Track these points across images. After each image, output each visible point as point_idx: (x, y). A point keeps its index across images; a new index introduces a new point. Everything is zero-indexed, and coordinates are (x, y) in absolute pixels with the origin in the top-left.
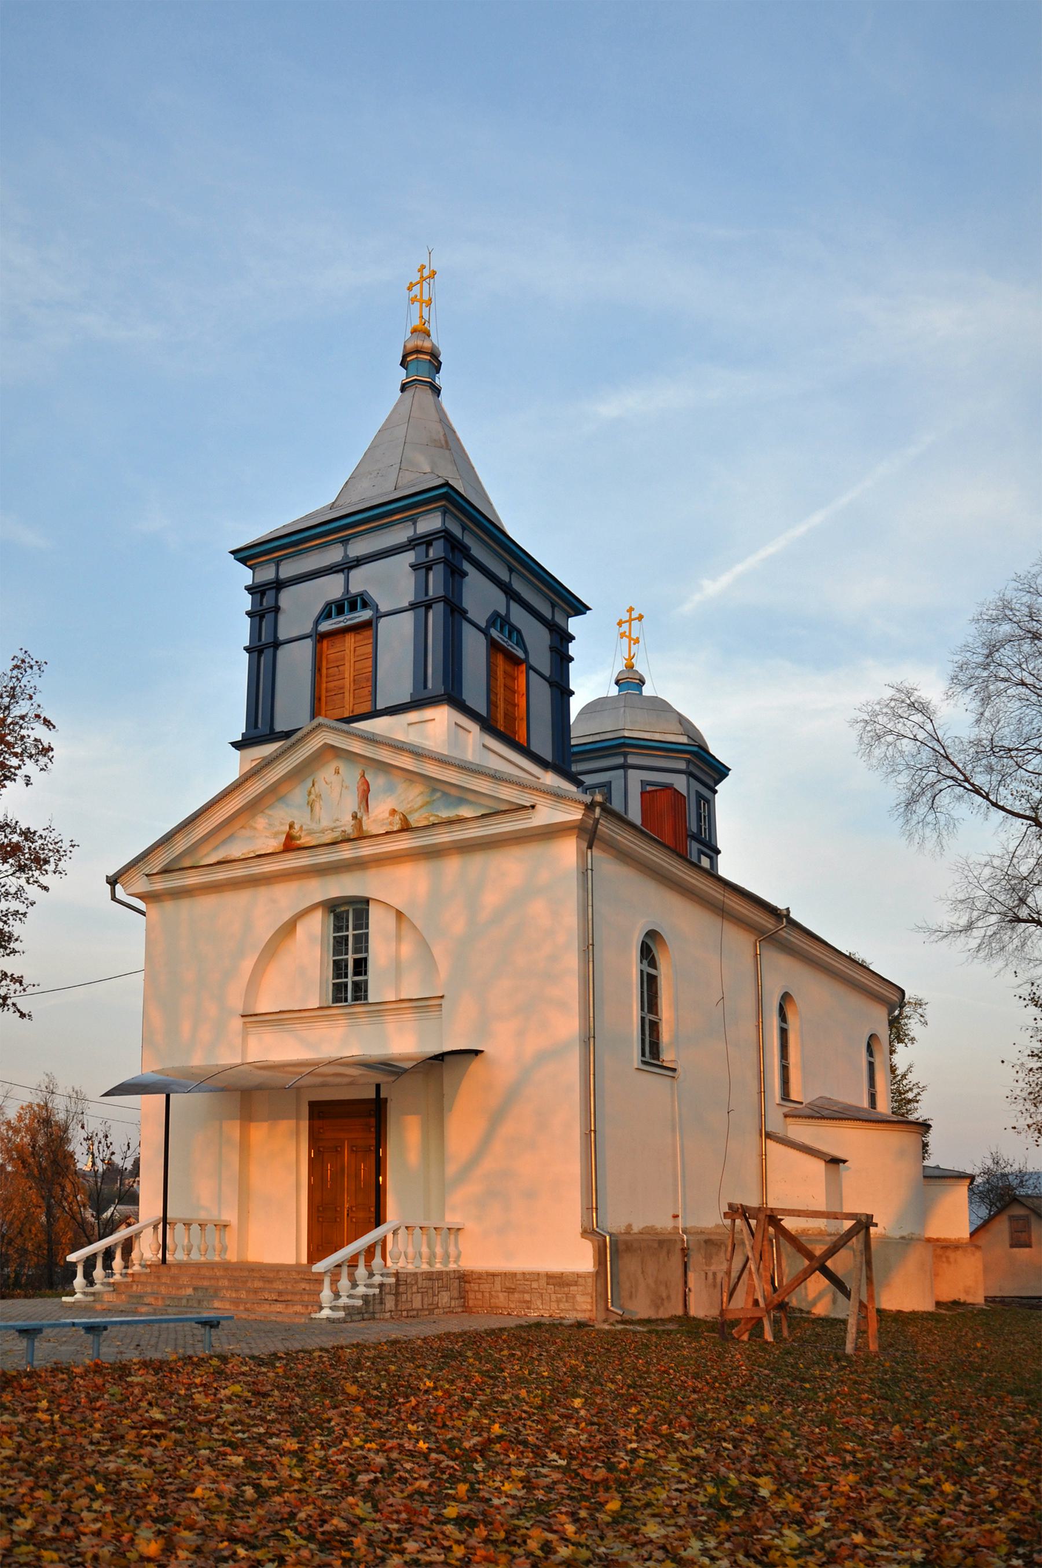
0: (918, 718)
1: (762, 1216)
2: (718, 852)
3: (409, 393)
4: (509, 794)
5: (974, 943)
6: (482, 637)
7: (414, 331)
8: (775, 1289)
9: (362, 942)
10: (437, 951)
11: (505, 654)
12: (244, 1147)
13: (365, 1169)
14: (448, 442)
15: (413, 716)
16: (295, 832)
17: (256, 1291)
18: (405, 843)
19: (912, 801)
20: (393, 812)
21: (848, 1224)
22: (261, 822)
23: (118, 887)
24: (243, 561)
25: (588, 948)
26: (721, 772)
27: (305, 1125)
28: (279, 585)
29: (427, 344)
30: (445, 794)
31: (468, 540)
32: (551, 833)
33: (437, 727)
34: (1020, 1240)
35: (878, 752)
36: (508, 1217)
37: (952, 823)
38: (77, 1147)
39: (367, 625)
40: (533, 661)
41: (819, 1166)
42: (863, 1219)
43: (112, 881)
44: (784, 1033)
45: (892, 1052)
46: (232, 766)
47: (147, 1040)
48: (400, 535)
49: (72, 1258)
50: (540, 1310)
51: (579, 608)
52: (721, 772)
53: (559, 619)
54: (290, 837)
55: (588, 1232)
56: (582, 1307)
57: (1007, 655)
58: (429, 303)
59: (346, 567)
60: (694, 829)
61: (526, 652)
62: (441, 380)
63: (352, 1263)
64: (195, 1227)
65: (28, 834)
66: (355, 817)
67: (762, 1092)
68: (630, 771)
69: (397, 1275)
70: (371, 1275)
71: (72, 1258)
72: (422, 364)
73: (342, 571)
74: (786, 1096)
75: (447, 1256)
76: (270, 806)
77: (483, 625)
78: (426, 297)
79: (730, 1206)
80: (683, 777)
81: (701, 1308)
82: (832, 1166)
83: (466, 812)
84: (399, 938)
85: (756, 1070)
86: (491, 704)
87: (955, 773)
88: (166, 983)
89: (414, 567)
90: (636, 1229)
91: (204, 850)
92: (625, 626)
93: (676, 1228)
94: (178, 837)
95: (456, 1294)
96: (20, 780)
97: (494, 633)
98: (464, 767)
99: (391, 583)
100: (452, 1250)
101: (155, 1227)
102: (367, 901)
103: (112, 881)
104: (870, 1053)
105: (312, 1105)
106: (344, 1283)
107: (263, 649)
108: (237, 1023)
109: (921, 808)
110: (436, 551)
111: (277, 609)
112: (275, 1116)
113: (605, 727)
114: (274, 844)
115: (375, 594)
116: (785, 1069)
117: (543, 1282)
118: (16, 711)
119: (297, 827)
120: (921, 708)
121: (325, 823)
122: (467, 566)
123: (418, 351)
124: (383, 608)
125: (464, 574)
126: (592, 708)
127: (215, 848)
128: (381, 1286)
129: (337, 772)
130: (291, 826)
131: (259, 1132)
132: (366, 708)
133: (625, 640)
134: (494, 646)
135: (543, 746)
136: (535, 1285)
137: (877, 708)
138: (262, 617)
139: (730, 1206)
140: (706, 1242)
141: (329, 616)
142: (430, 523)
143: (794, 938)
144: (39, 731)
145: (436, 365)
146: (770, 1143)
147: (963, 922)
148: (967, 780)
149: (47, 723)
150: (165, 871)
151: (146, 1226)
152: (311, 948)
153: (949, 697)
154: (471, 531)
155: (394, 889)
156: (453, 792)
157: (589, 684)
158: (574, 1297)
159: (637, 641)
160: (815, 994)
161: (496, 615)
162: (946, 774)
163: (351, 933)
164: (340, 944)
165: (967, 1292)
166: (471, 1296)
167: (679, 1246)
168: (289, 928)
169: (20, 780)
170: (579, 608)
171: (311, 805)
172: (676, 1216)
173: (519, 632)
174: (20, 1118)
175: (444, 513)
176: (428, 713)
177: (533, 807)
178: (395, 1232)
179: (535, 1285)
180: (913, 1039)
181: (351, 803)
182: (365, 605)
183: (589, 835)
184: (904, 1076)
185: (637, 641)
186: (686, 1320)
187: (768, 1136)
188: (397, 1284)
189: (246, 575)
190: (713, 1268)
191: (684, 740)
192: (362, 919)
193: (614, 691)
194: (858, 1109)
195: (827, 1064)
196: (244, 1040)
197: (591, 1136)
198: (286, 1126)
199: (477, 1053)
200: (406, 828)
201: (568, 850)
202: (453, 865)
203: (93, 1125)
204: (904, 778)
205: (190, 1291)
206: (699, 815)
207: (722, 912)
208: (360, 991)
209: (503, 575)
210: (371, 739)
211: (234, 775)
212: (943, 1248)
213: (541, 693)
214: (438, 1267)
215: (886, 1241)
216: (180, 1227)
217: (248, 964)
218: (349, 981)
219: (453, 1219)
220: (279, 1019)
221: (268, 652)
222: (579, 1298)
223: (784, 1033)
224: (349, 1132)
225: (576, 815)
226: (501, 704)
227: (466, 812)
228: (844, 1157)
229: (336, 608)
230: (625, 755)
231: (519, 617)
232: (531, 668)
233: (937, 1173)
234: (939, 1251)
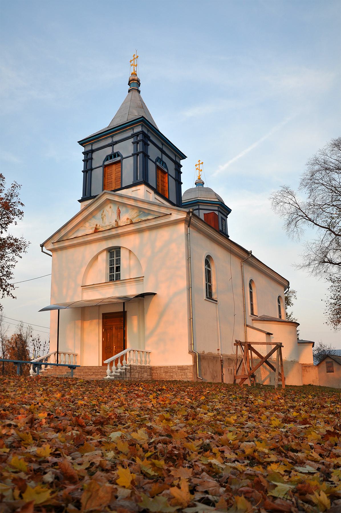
0: (290, 197)
1: (246, 345)
3: (131, 93)
4: (163, 211)
5: (311, 270)
7: (132, 74)
8: (251, 369)
9: (118, 261)
10: (142, 262)
11: (161, 170)
12: (82, 329)
13: (120, 335)
14: (143, 106)
15: (134, 188)
16: (98, 227)
17: (86, 372)
18: (132, 228)
19: (289, 224)
20: (128, 219)
21: (274, 346)
22: (87, 225)
23: (44, 247)
24: (81, 144)
25: (189, 259)
26: (229, 211)
27: (101, 321)
28: (92, 151)
29: (136, 78)
30: (144, 212)
31: (149, 135)
32: (176, 222)
33: (141, 192)
34: (330, 370)
35: (278, 208)
36: (164, 346)
37: (302, 231)
38: (30, 348)
39: (119, 162)
40: (169, 173)
42: (279, 344)
43: (42, 246)
44: (251, 293)
45: (286, 308)
46: (79, 207)
47: (52, 295)
48: (129, 134)
50: (176, 378)
51: (184, 157)
52: (229, 211)
53: (177, 160)
54: (96, 229)
55: (190, 352)
56: (189, 377)
57: (318, 175)
58: (136, 66)
60: (221, 229)
61: (167, 170)
62: (140, 88)
63: (116, 361)
64: (67, 355)
65: (16, 240)
66: (116, 221)
67: (245, 311)
69: (130, 366)
70: (122, 366)
72: (134, 84)
74: (252, 314)
75: (146, 361)
76: (90, 219)
77: (154, 161)
78: (135, 64)
79: (236, 341)
81: (228, 380)
83: (150, 217)
84: (130, 259)
85: (243, 304)
86: (157, 185)
87: (302, 214)
88: (58, 278)
89: (133, 143)
90: (206, 353)
91: (70, 234)
93: (219, 354)
94: (62, 230)
96: (14, 223)
97: (158, 163)
98: (150, 203)
99: (127, 148)
100: (147, 359)
101: (55, 354)
102: (119, 248)
103: (42, 246)
104: (279, 302)
105: (103, 314)
106: (114, 367)
107: (88, 171)
108: (80, 289)
109: (292, 226)
110: (140, 137)
111: (92, 159)
112: (92, 318)
113: (192, 197)
114: (92, 231)
115: (121, 152)
116: (252, 305)
117: (177, 369)
118: (12, 201)
119: (98, 225)
120: (291, 193)
121: (107, 223)
122: (149, 143)
123: (133, 80)
124: (124, 156)
125: (149, 145)
126: (188, 192)
127: (73, 234)
128: (126, 369)
129: (110, 208)
130: (96, 225)
131: (87, 324)
132: (119, 187)
133: (198, 171)
134: (158, 167)
135: (173, 199)
136: (174, 370)
137: (277, 194)
138: (87, 161)
139: (236, 341)
140: (228, 359)
141: (107, 160)
142: (138, 129)
143: (254, 261)
144: (19, 207)
145: (139, 84)
147: (307, 263)
148: (306, 216)
149: (22, 204)
150: (58, 241)
151: (52, 354)
152: (103, 264)
153: (300, 189)
154: (151, 132)
155: (127, 243)
156: (146, 211)
157: (187, 184)
158: (187, 373)
159: (201, 171)
160: (261, 281)
161: (158, 158)
162: (299, 215)
163: (115, 258)
164: (111, 262)
165: (313, 382)
166: (154, 375)
167: (220, 359)
168: (96, 258)
169: (14, 223)
170: (184, 157)
171: (103, 218)
172: (218, 350)
173: (165, 164)
174: (12, 339)
175: (142, 126)
176: (138, 187)
177: (171, 214)
178: (130, 352)
179: (174, 370)
180: (292, 304)
181: (115, 217)
182: (118, 156)
183: (188, 223)
184: (290, 316)
185: (201, 171)
186: (222, 384)
187: (247, 326)
188: (131, 369)
189: (83, 149)
190: (231, 368)
191: (217, 200)
192: (118, 254)
193: (195, 186)
194: (276, 318)
195: (266, 306)
196: (82, 294)
197: (191, 320)
198: (95, 321)
199: (155, 294)
200: (132, 223)
201: (182, 228)
202: (146, 235)
203: (35, 336)
204: (286, 217)
205: (66, 373)
206: (222, 224)
207: (231, 251)
208: (118, 278)
209: (160, 146)
210: (121, 196)
211: (79, 210)
212: (305, 367)
213: (172, 183)
214: (143, 365)
215: (287, 362)
216: (62, 355)
217: (83, 270)
218: (115, 273)
219: (148, 349)
220: (93, 287)
221: (89, 172)
222: (188, 374)
223: (251, 293)
224: (115, 321)
225: (184, 216)
226: (160, 186)
227: (150, 217)
230: (199, 205)
231: (165, 159)
232: (169, 175)
233: (302, 342)
234: (304, 368)
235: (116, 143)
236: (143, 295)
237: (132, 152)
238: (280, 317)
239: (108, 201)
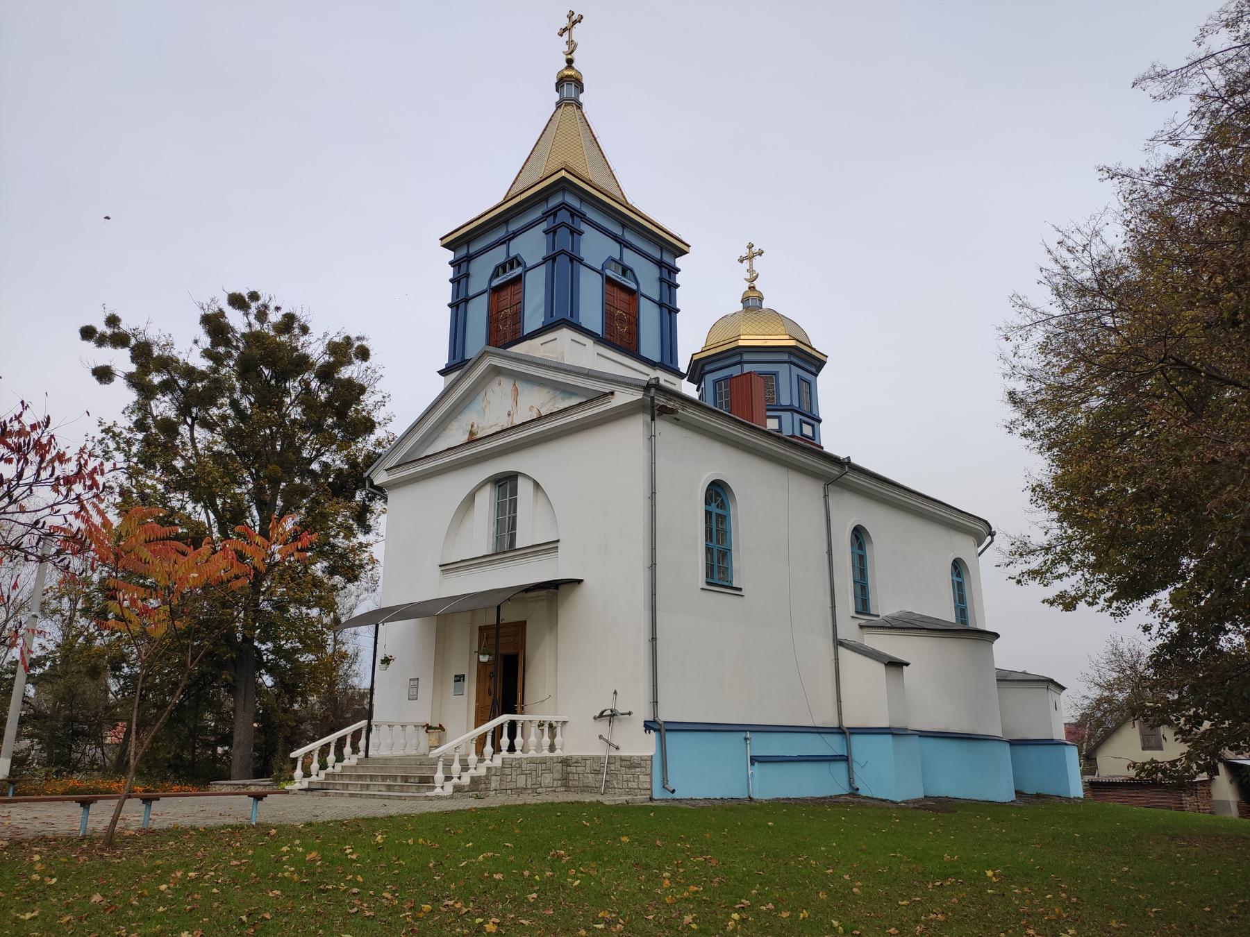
2: (819, 421)
9: (514, 503)
39: (519, 280)
40: (643, 290)
41: (880, 668)
48: (537, 214)
53: (667, 258)
54: (471, 433)
59: (507, 240)
61: (637, 283)
71: (293, 755)
82: (894, 670)
95: (558, 776)
97: (609, 273)
99: (531, 246)
107: (459, 305)
111: (467, 275)
117: (618, 764)
124: (528, 265)
134: (609, 281)
141: (498, 276)
146: (841, 649)
160: (886, 529)
173: (632, 271)
177: (612, 393)
182: (519, 264)
189: (450, 255)
199: (580, 581)
209: (617, 230)
216: (385, 728)
228: (906, 660)
229: (501, 268)
230: (741, 354)
231: (630, 258)
235: (515, 235)
237: (544, 254)
239: (497, 371)
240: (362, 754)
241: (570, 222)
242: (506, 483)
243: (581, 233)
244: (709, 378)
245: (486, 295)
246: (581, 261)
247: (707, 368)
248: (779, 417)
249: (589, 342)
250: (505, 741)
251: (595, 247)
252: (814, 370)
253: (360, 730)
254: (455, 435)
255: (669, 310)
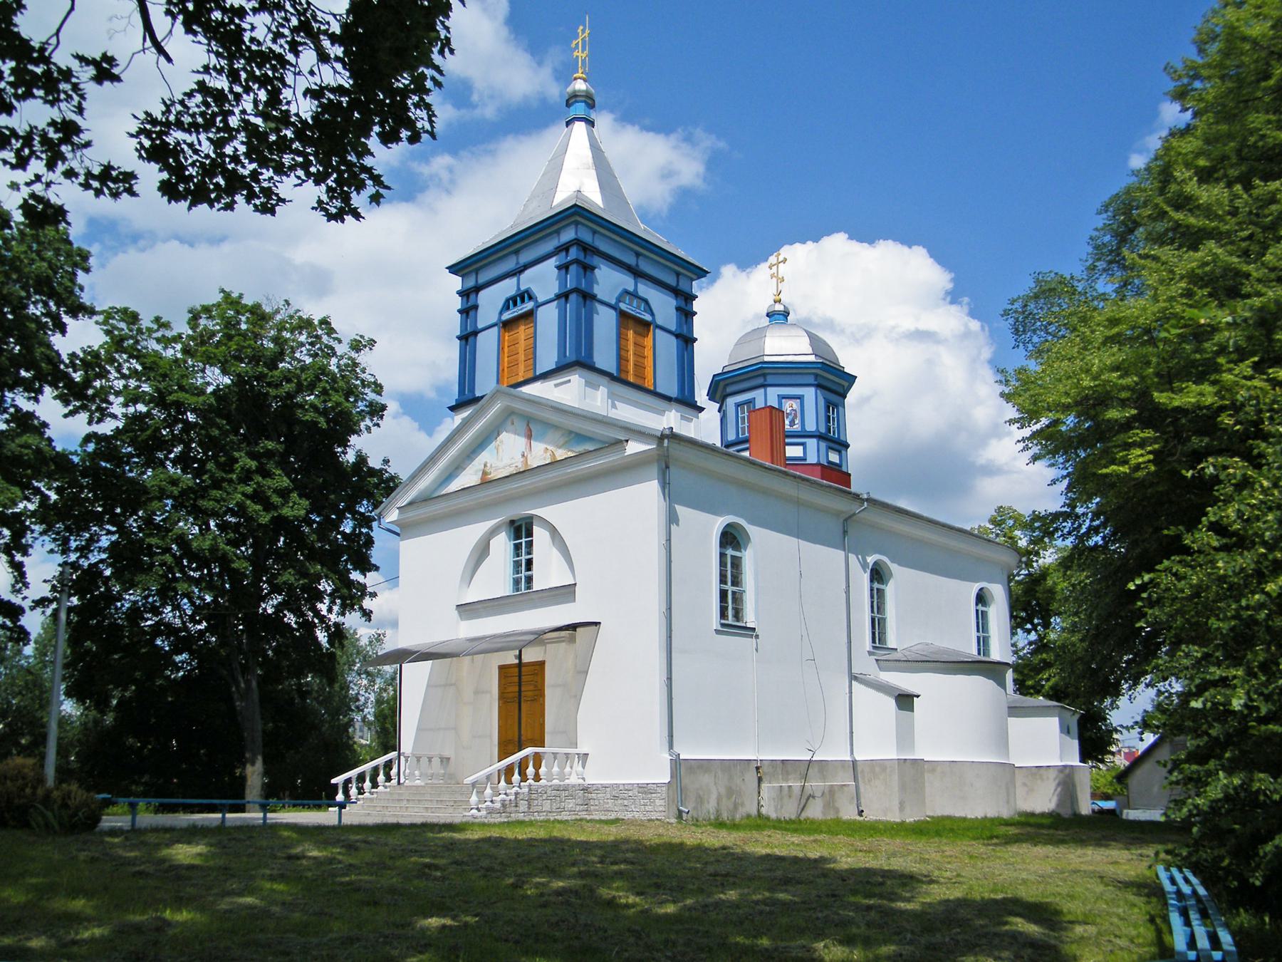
2: (847, 446)
6: (613, 313)
11: (634, 323)
16: (488, 470)
49: (333, 781)
53: (683, 285)
54: (485, 473)
61: (652, 314)
64: (424, 761)
68: (769, 389)
71: (333, 781)
73: (514, 275)
80: (812, 390)
89: (559, 268)
92: (774, 268)
97: (623, 306)
99: (544, 279)
110: (574, 253)
111: (476, 307)
121: (506, 461)
124: (540, 300)
132: (530, 375)
134: (623, 315)
135: (668, 385)
141: (508, 308)
168: (482, 551)
182: (530, 298)
189: (456, 282)
191: (812, 358)
209: (630, 259)
213: (667, 346)
228: (916, 692)
229: (512, 301)
230: (764, 375)
236: (573, 627)
237: (556, 291)
238: (983, 643)
240: (394, 782)
241: (581, 257)
242: (521, 530)
243: (593, 268)
244: (731, 401)
245: (495, 329)
246: (594, 297)
247: (729, 390)
248: (803, 444)
249: (605, 380)
250: (530, 771)
251: (609, 282)
252: (841, 390)
253: (391, 761)
254: (469, 478)
255: (686, 340)
